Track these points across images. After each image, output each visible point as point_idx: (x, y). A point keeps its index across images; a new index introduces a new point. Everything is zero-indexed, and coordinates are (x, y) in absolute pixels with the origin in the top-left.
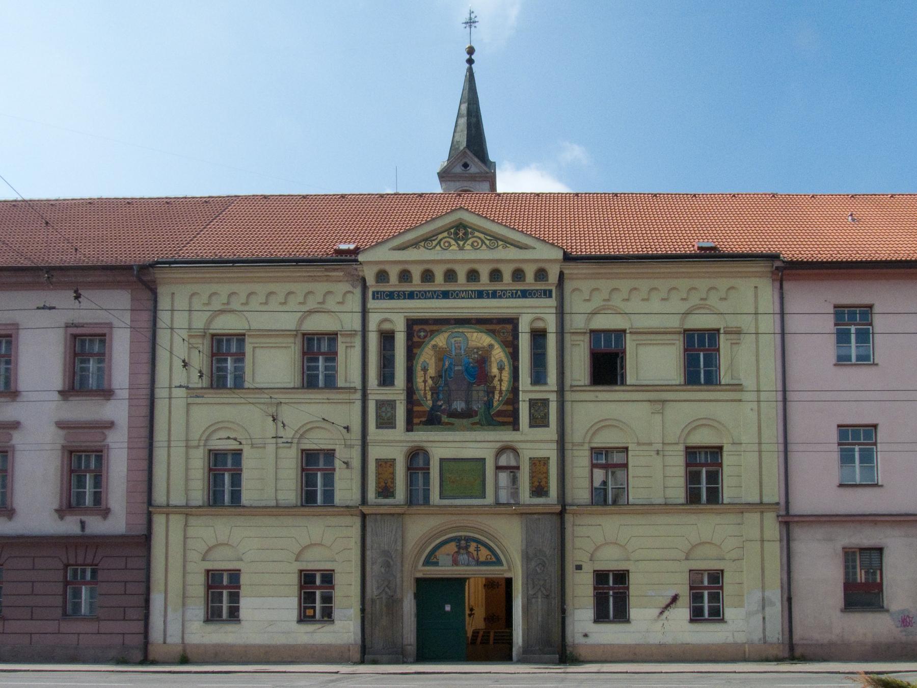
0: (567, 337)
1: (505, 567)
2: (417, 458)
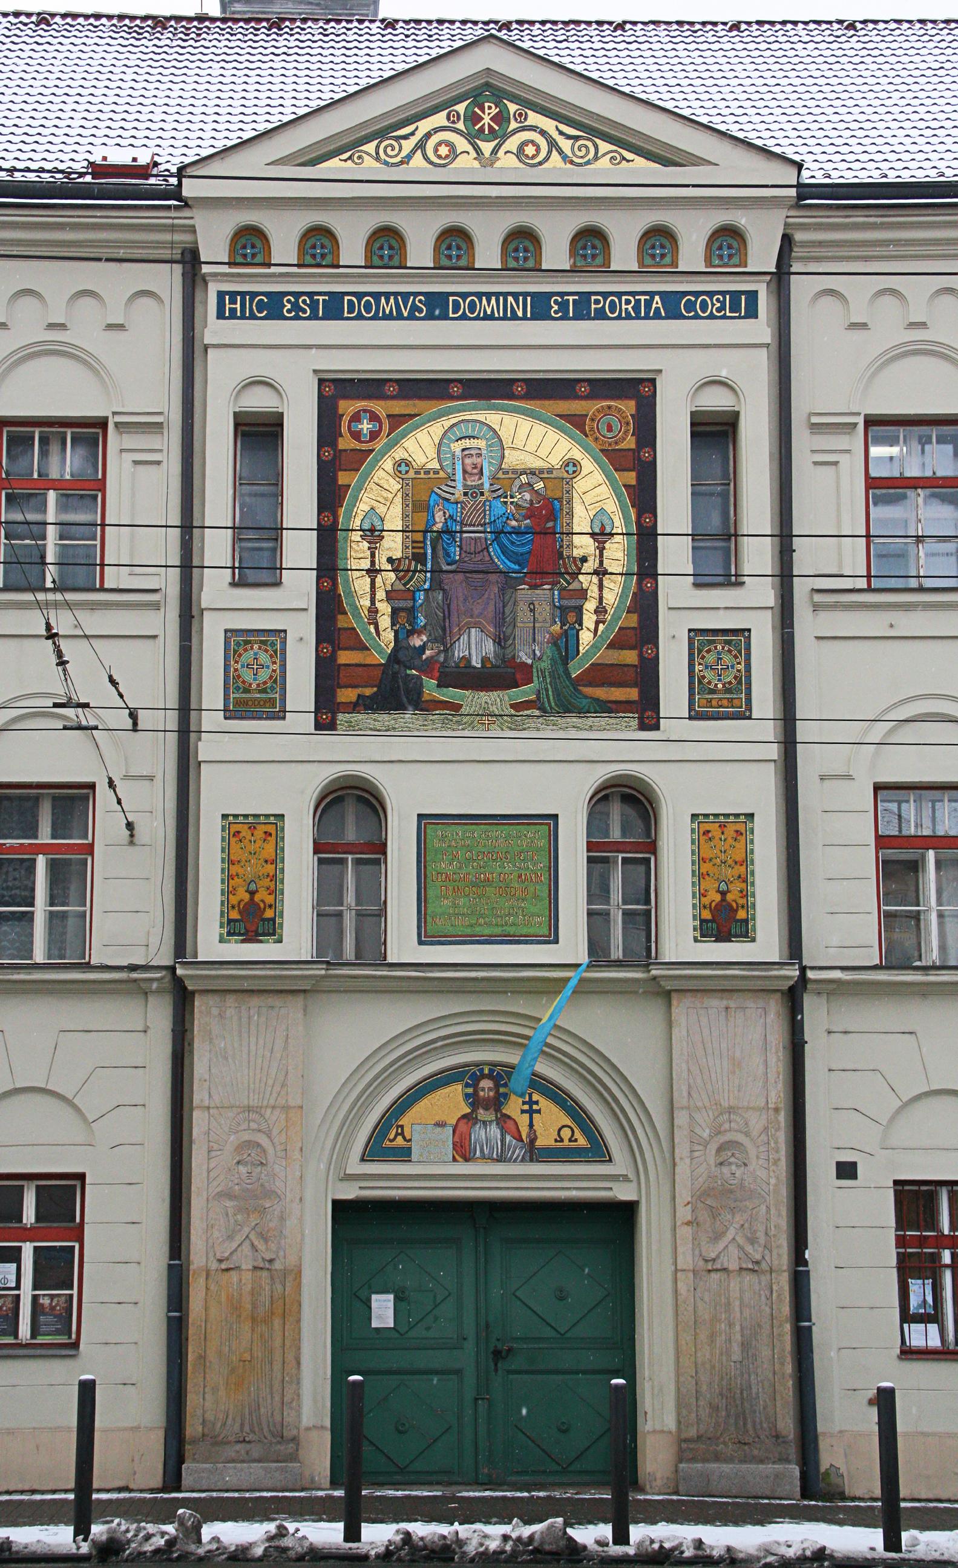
0: (802, 441)
1: (621, 1164)
2: (352, 806)
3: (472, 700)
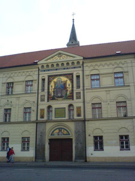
2: (49, 107)
3: (59, 99)
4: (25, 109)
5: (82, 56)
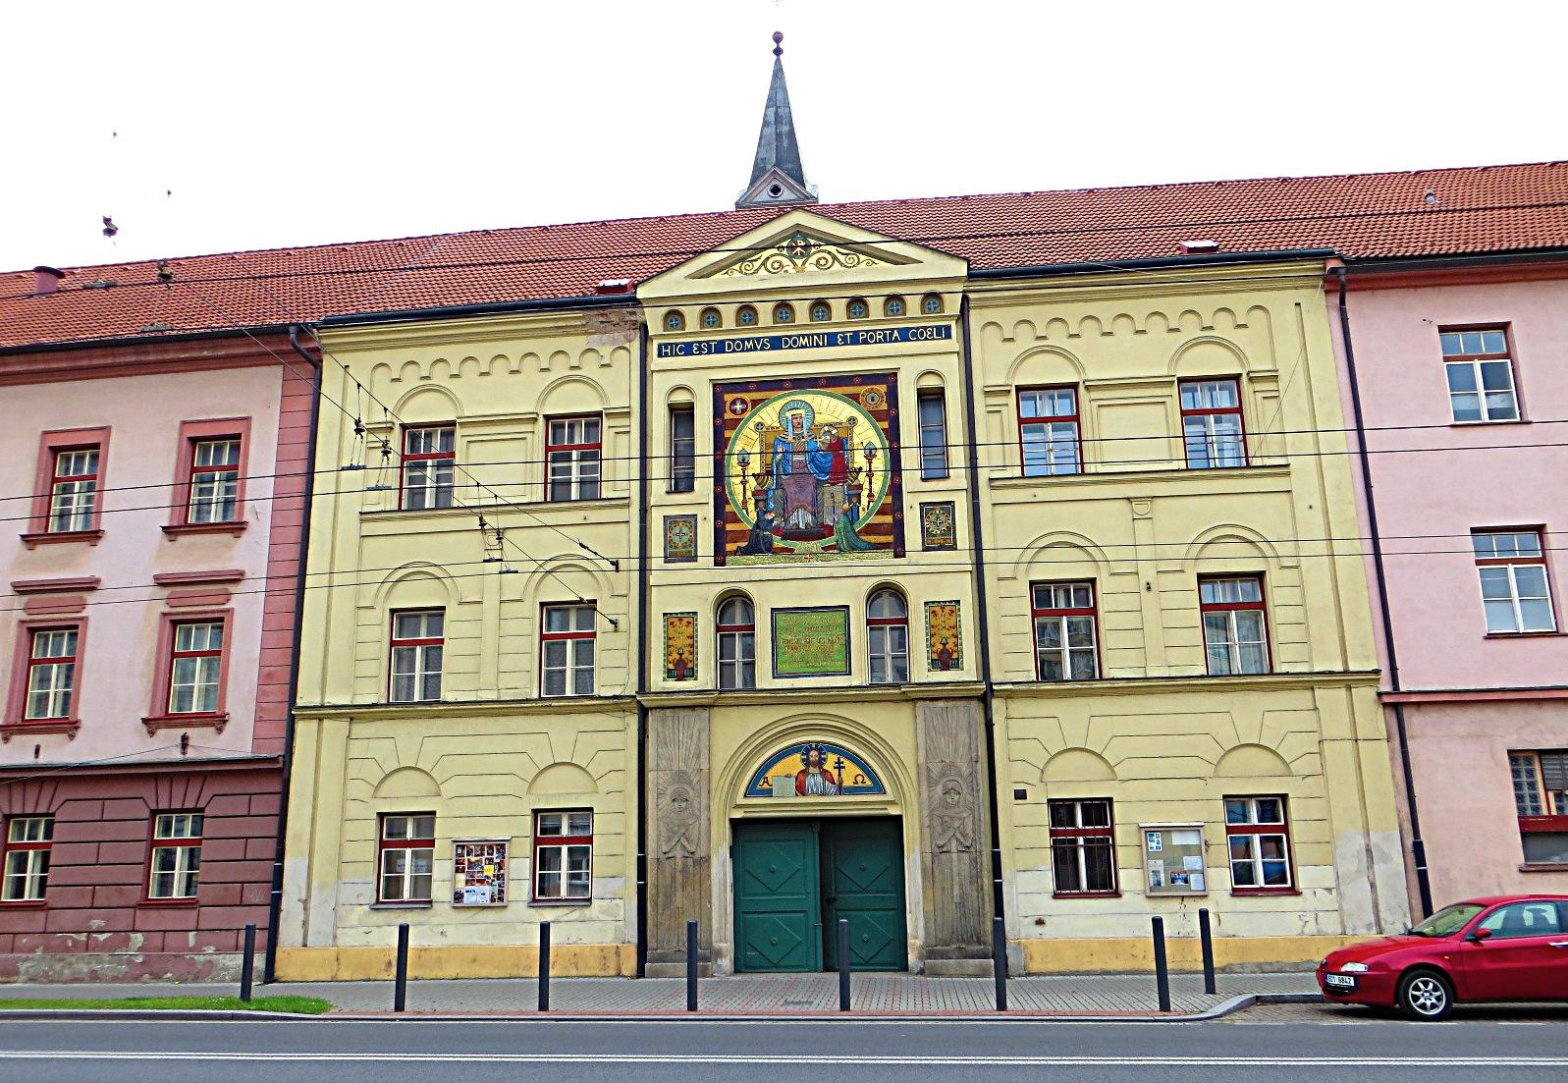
2: (733, 604)
4: (401, 619)
5: (957, 257)
